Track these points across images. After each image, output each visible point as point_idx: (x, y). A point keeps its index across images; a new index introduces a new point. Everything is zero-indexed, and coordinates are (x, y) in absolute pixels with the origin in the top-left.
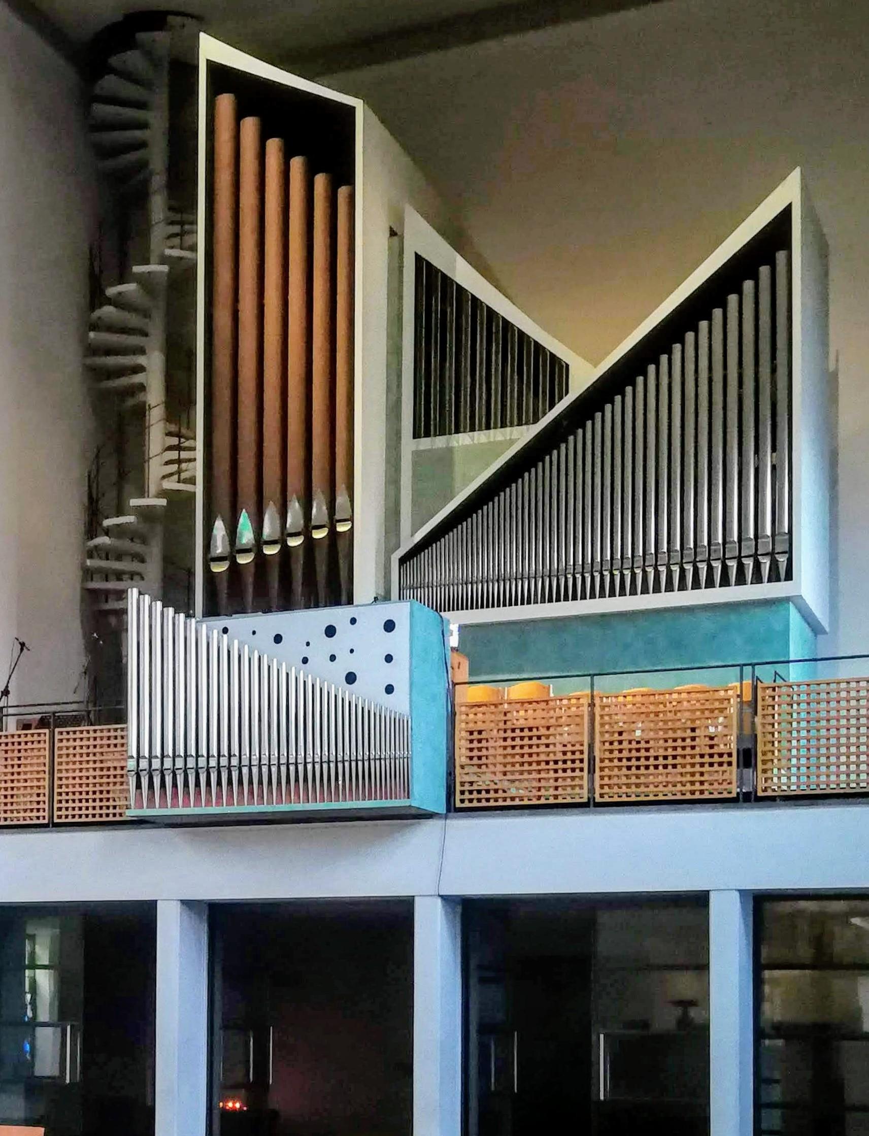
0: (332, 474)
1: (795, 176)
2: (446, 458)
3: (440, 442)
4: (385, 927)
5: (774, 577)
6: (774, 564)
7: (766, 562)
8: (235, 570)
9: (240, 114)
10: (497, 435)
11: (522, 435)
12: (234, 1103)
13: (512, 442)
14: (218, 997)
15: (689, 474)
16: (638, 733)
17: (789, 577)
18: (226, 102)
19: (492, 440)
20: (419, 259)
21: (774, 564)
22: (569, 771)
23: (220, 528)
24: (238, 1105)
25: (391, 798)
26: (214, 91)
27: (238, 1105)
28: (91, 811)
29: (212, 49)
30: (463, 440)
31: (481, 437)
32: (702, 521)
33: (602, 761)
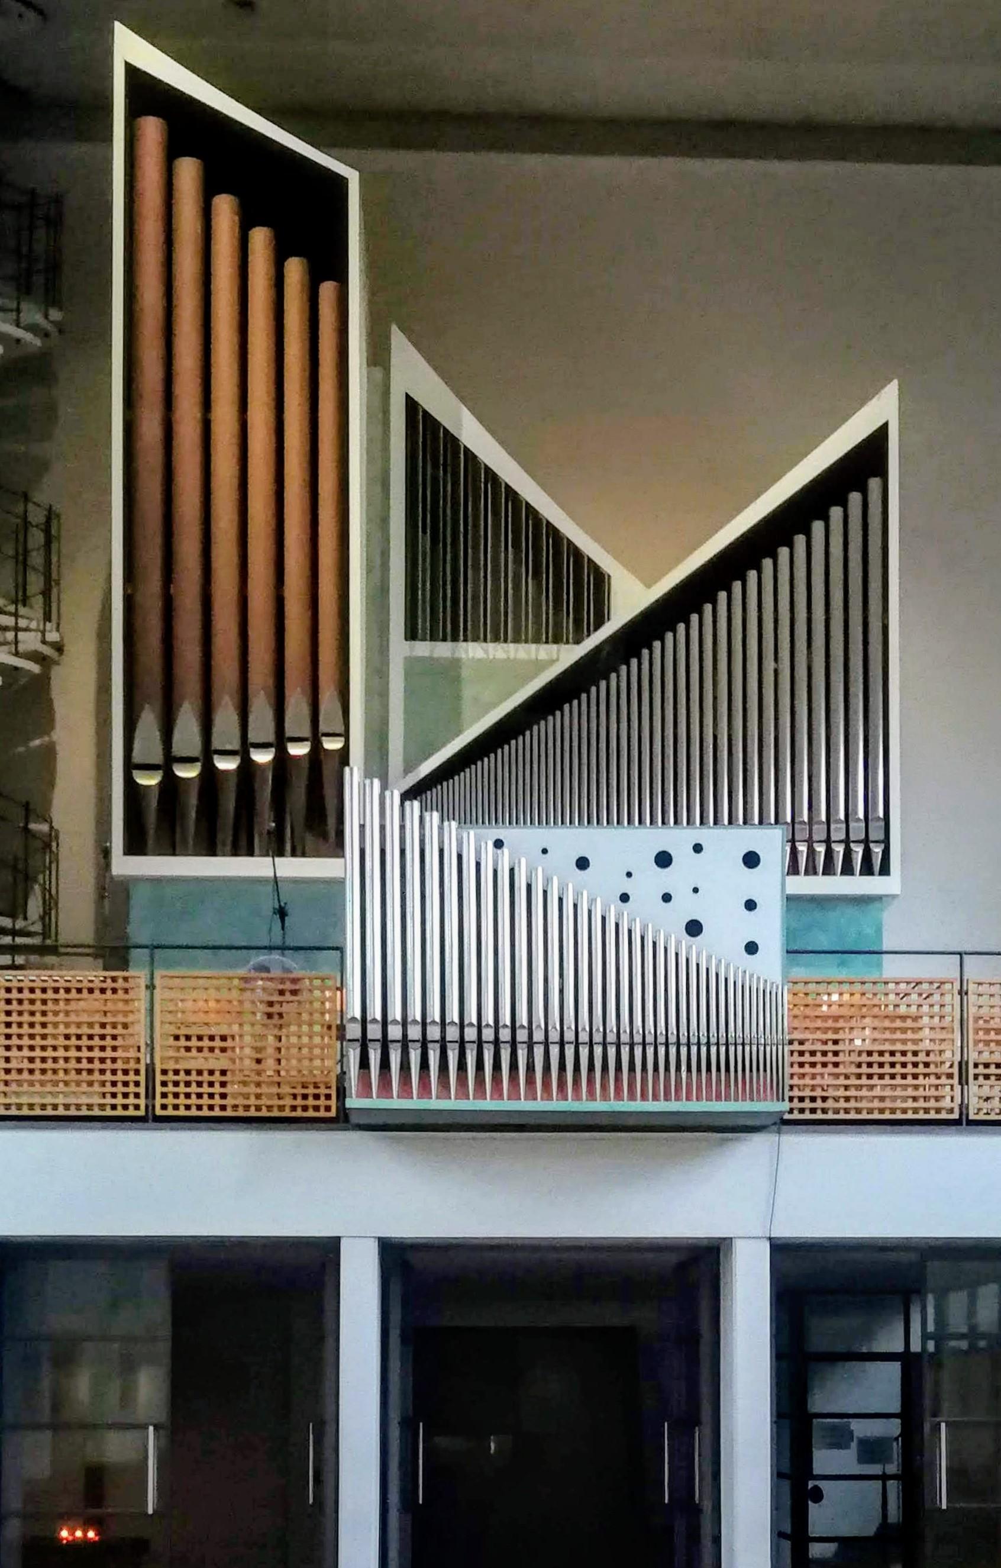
0: (323, 675)
1: (892, 390)
2: (450, 673)
3: (443, 650)
4: (698, 1267)
5: (867, 869)
6: (867, 855)
7: (858, 850)
8: (171, 785)
9: (173, 151)
10: (544, 651)
11: (568, 655)
12: (85, 1533)
13: (552, 662)
14: (395, 1365)
15: (819, 735)
16: (858, 1042)
17: (885, 870)
18: (152, 128)
19: (512, 656)
20: (412, 405)
21: (867, 855)
22: (910, 1077)
23: (149, 721)
24: (91, 1534)
25: (772, 1100)
26: (133, 114)
27: (64, 1534)
28: (182, 1100)
29: (131, 49)
30: (472, 651)
31: (498, 651)
32: (856, 792)
33: (976, 1066)
